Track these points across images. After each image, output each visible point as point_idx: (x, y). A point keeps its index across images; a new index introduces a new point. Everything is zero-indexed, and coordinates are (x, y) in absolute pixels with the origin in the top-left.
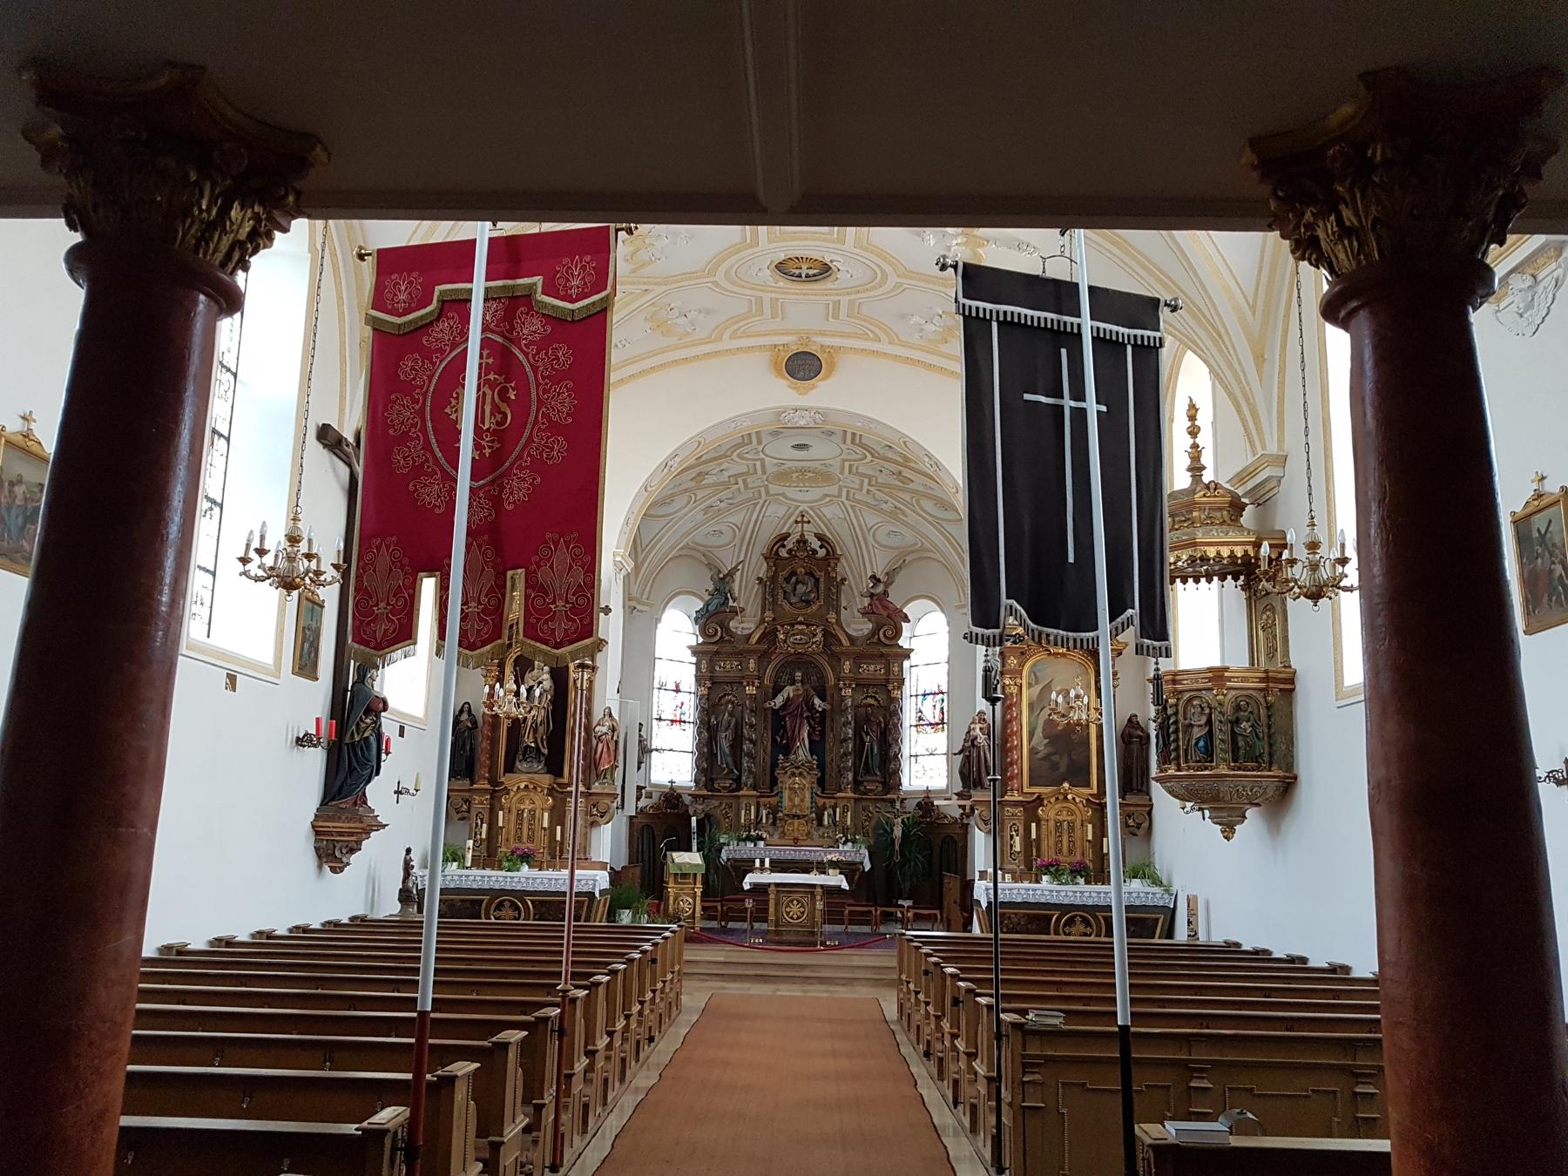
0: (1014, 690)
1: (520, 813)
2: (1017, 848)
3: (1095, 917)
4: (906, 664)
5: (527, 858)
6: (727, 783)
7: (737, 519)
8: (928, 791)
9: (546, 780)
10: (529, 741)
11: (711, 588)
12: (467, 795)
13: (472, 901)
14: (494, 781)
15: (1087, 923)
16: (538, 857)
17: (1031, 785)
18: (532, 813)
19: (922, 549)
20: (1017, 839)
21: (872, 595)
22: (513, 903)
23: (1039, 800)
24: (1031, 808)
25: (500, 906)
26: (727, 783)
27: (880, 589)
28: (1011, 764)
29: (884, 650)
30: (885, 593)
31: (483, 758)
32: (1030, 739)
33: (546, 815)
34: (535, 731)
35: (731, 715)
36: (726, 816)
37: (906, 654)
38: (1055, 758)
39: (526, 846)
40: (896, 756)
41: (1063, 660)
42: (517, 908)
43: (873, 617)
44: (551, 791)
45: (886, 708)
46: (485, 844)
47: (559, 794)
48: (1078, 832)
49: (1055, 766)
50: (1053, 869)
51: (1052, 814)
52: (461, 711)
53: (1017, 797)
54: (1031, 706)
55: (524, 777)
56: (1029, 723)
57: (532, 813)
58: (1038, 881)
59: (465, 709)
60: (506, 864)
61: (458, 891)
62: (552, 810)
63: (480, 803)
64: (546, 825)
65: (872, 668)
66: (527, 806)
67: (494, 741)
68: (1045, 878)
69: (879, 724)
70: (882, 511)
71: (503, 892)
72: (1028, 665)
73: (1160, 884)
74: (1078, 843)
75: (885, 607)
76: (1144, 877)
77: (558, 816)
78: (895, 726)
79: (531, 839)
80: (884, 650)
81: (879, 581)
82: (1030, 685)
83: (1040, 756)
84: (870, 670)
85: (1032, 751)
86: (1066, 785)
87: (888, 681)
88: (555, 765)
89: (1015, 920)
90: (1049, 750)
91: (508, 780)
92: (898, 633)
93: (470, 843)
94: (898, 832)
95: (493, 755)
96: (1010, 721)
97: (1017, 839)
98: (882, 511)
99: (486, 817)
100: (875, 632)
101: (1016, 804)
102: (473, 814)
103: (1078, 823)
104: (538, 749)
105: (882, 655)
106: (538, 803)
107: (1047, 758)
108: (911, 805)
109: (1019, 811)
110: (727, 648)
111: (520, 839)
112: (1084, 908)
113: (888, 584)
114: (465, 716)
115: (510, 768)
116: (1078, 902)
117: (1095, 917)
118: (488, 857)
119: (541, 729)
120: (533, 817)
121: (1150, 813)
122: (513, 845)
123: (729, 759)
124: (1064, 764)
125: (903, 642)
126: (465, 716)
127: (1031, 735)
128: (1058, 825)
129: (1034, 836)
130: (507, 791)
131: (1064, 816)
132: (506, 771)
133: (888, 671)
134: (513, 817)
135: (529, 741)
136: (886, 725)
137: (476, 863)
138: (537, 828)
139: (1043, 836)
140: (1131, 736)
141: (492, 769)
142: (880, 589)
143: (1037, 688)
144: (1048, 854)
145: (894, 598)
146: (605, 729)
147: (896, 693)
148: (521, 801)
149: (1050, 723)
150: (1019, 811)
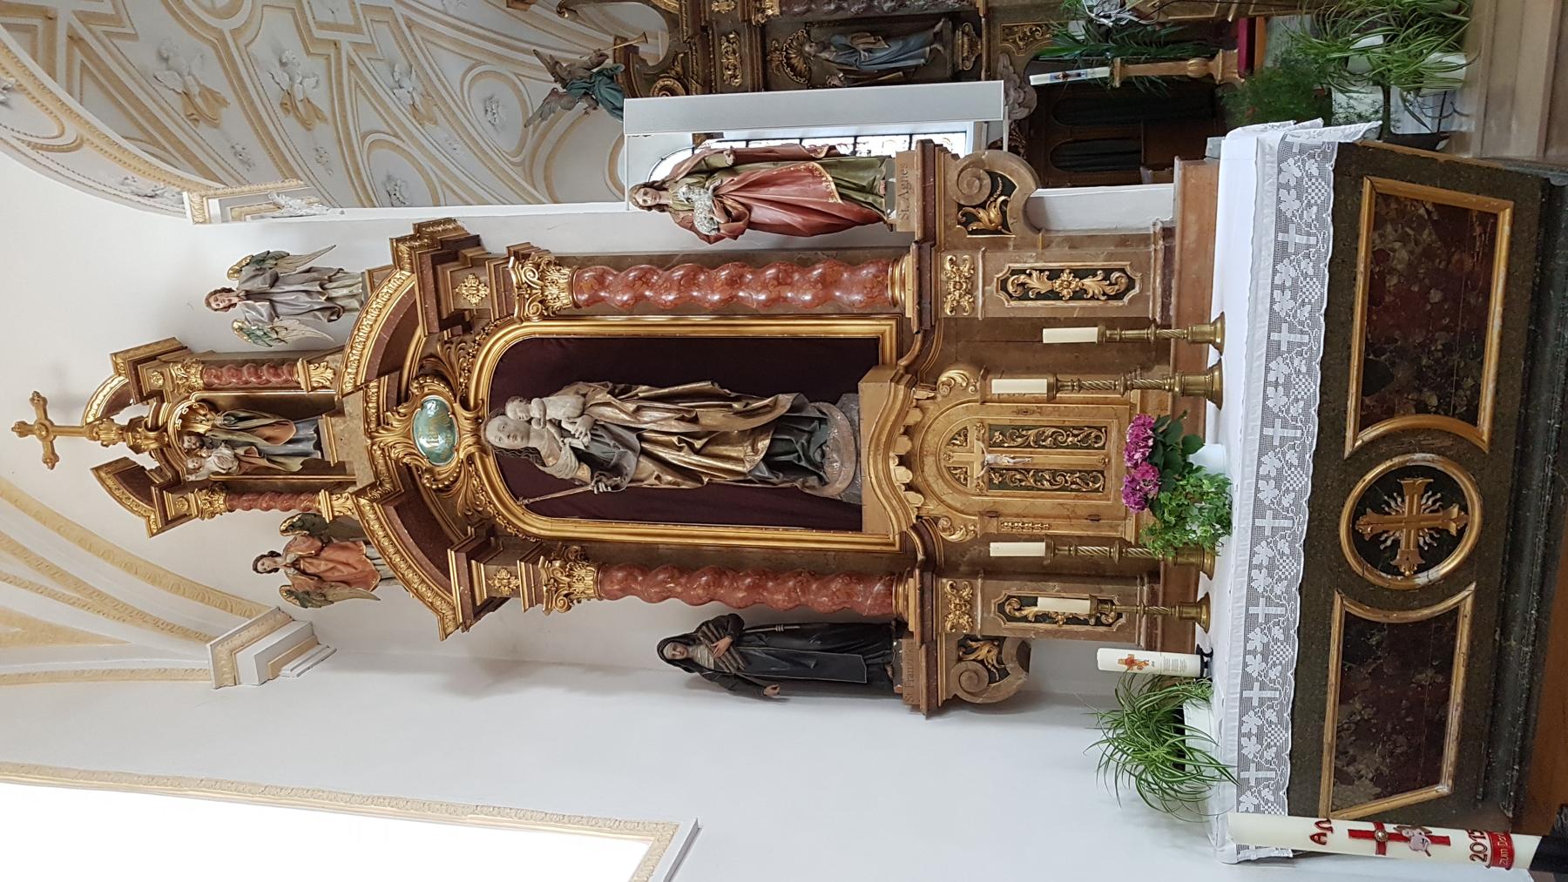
1: (999, 478)
5: (1169, 453)
6: (962, 40)
7: (452, 67)
9: (877, 396)
10: (747, 459)
11: (582, 105)
12: (943, 649)
13: (1349, 654)
14: (895, 566)
16: (1159, 406)
18: (997, 436)
20: (1045, 604)
22: (1373, 500)
25: (1374, 551)
26: (962, 40)
31: (824, 600)
33: (1001, 386)
34: (716, 437)
35: (825, 47)
36: (1029, 39)
39: (1118, 454)
42: (1390, 485)
44: (921, 374)
46: (1109, 591)
47: (936, 344)
52: (688, 664)
55: (871, 472)
57: (997, 436)
59: (679, 652)
60: (1197, 530)
61: (1304, 714)
62: (986, 369)
63: (968, 608)
64: (1036, 386)
66: (975, 457)
67: (775, 566)
71: (1318, 543)
77: (1007, 344)
79: (1090, 437)
88: (835, 368)
91: (885, 523)
93: (1110, 658)
95: (816, 568)
99: (1014, 588)
102: (1007, 629)
104: (779, 425)
106: (961, 416)
110: (696, 66)
111: (1091, 477)
114: (702, 654)
115: (846, 515)
118: (1164, 591)
119: (713, 417)
120: (1012, 433)
122: (1113, 496)
123: (914, 41)
126: (702, 654)
130: (924, 525)
132: (857, 527)
134: (1013, 501)
135: (747, 459)
137: (1178, 621)
138: (1049, 418)
141: (858, 569)
146: (702, 200)
148: (957, 475)
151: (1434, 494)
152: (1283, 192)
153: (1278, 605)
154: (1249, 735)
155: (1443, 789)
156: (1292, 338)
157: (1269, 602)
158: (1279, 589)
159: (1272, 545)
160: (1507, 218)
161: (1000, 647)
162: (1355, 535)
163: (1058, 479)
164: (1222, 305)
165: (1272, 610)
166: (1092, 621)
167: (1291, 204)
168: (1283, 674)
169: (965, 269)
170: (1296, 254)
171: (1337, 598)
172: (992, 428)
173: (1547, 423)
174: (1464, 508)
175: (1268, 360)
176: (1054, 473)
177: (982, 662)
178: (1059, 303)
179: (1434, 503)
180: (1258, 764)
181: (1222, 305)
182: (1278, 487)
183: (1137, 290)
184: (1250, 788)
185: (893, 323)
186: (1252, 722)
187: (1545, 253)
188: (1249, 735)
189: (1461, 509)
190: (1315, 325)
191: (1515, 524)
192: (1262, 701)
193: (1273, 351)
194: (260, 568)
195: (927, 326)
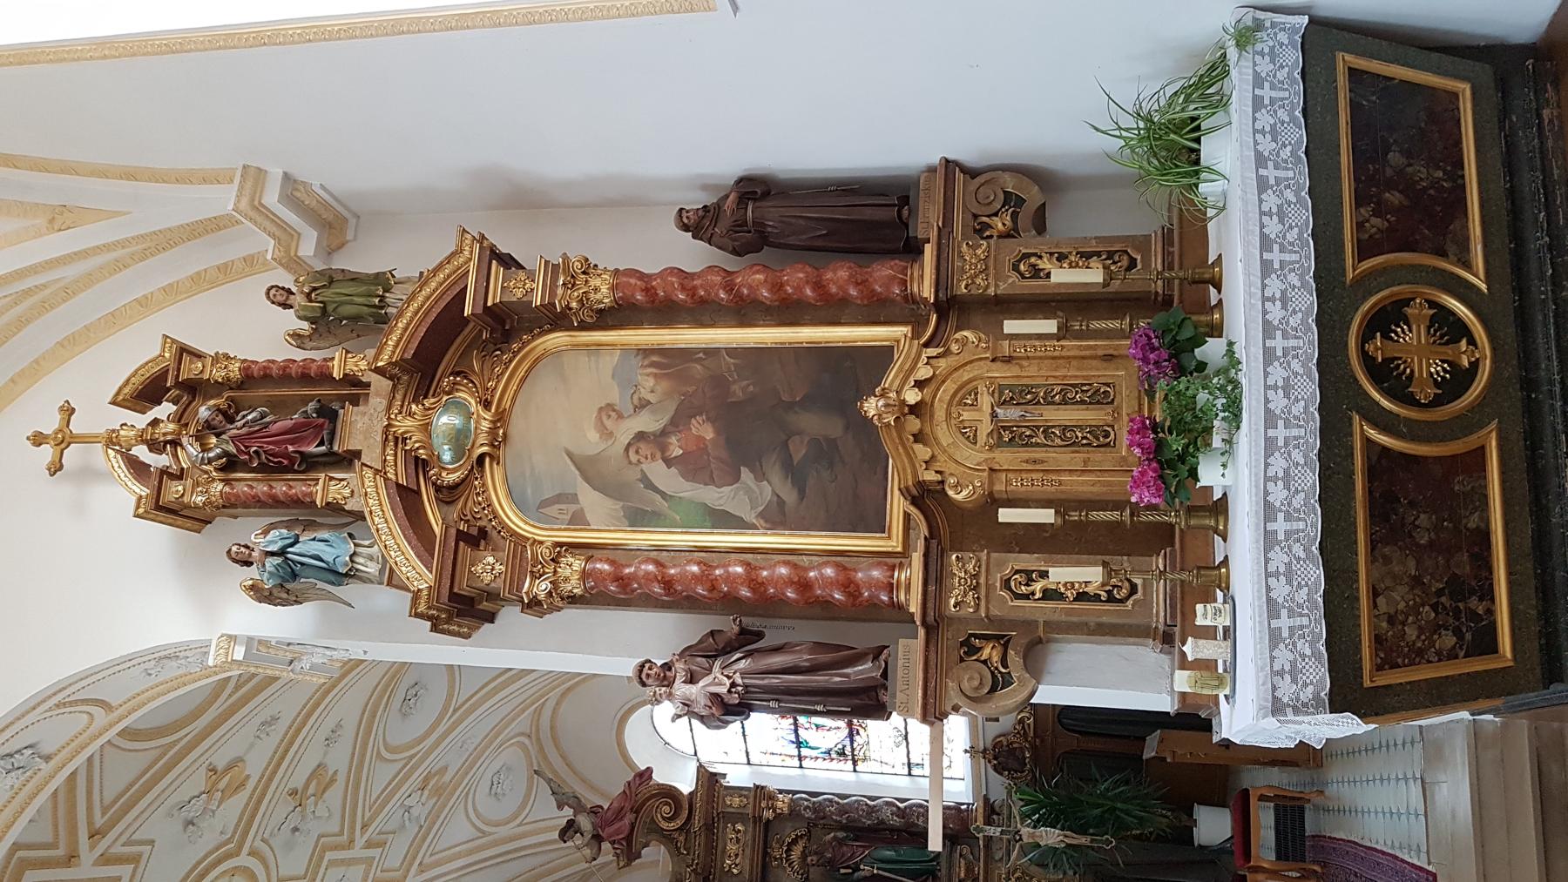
0: (573, 566)
2: (1090, 575)
3: (1365, 285)
4: (738, 777)
8: (972, 751)
15: (1385, 320)
17: (878, 525)
19: (533, 734)
20: (1061, 575)
21: (597, 838)
23: (925, 497)
24: (949, 524)
25: (1386, 374)
27: (585, 822)
28: (804, 586)
29: (697, 823)
30: (595, 811)
32: (740, 524)
37: (709, 780)
38: (799, 451)
40: (901, 813)
41: (517, 425)
43: (639, 838)
45: (811, 825)
48: (1032, 374)
49: (825, 452)
50: (1173, 449)
51: (972, 456)
53: (913, 572)
54: (639, 518)
56: (687, 526)
58: (1220, 508)
65: (732, 848)
68: (1210, 475)
69: (841, 842)
70: (433, 817)
72: (514, 519)
73: (1217, 70)
74: (1073, 374)
75: (619, 814)
76: (1193, 128)
78: (843, 810)
80: (697, 823)
81: (571, 823)
82: (578, 520)
83: (789, 496)
84: (736, 852)
85: (776, 518)
86: (871, 406)
87: (757, 819)
89: (1400, 598)
90: (776, 474)
92: (669, 793)
94: (1051, 837)
96: (668, 584)
97: (1061, 575)
98: (433, 817)
100: (667, 838)
101: (935, 576)
103: (1000, 373)
105: (709, 827)
107: (794, 473)
108: (999, 787)
109: (960, 566)
111: (1100, 437)
112: (1329, 324)
113: (578, 807)
116: (1308, 344)
117: (1365, 285)
121: (971, 173)
124: (815, 424)
125: (686, 784)
127: (723, 520)
128: (1007, 436)
129: (1046, 516)
131: (981, 416)
133: (739, 817)
136: (843, 828)
139: (1049, 490)
140: (740, 225)
142: (585, 822)
143: (590, 499)
144: (1114, 473)
145: (608, 789)
147: (782, 803)
149: (694, 466)
150: (960, 566)
151: (1440, 328)
152: (1259, 137)
153: (1291, 252)
154: (1275, 388)
155: (1465, 89)
156: (1274, 94)
157: (1285, 336)
158: (1294, 321)
159: (1283, 278)
160: (1494, 443)
161: (1005, 647)
162: (1367, 359)
163: (1068, 437)
164: (1219, 246)
165: (1287, 257)
166: (1104, 595)
167: (1266, 145)
168: (1304, 321)
169: (970, 567)
170: (1278, 184)
171: (1340, 55)
172: (1001, 388)
173: (1549, 366)
174: (1472, 342)
175: (1264, 277)
176: (1065, 429)
177: (984, 662)
178: (1062, 605)
179: (1442, 337)
180: (1281, 245)
181: (1219, 246)
182: (1287, 396)
183: (1139, 595)
184: (1278, 359)
185: (899, 549)
186: (1271, 202)
187: (1540, 512)
188: (1275, 388)
189: (1469, 343)
190: (1305, 244)
191: (1527, 357)
192: (1285, 351)
193: (1266, 268)
194: (273, 292)
195: (930, 619)
